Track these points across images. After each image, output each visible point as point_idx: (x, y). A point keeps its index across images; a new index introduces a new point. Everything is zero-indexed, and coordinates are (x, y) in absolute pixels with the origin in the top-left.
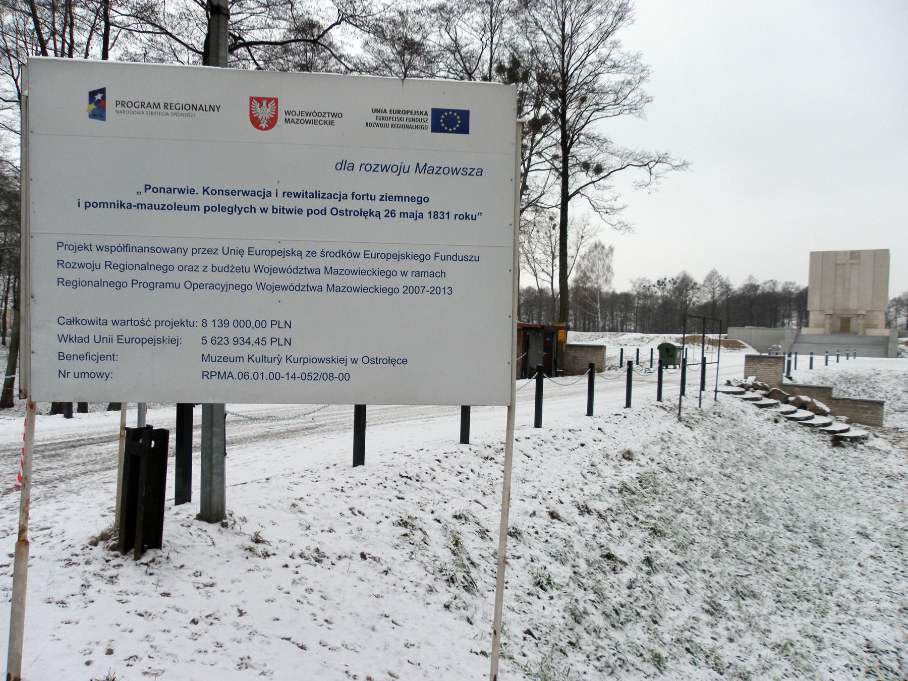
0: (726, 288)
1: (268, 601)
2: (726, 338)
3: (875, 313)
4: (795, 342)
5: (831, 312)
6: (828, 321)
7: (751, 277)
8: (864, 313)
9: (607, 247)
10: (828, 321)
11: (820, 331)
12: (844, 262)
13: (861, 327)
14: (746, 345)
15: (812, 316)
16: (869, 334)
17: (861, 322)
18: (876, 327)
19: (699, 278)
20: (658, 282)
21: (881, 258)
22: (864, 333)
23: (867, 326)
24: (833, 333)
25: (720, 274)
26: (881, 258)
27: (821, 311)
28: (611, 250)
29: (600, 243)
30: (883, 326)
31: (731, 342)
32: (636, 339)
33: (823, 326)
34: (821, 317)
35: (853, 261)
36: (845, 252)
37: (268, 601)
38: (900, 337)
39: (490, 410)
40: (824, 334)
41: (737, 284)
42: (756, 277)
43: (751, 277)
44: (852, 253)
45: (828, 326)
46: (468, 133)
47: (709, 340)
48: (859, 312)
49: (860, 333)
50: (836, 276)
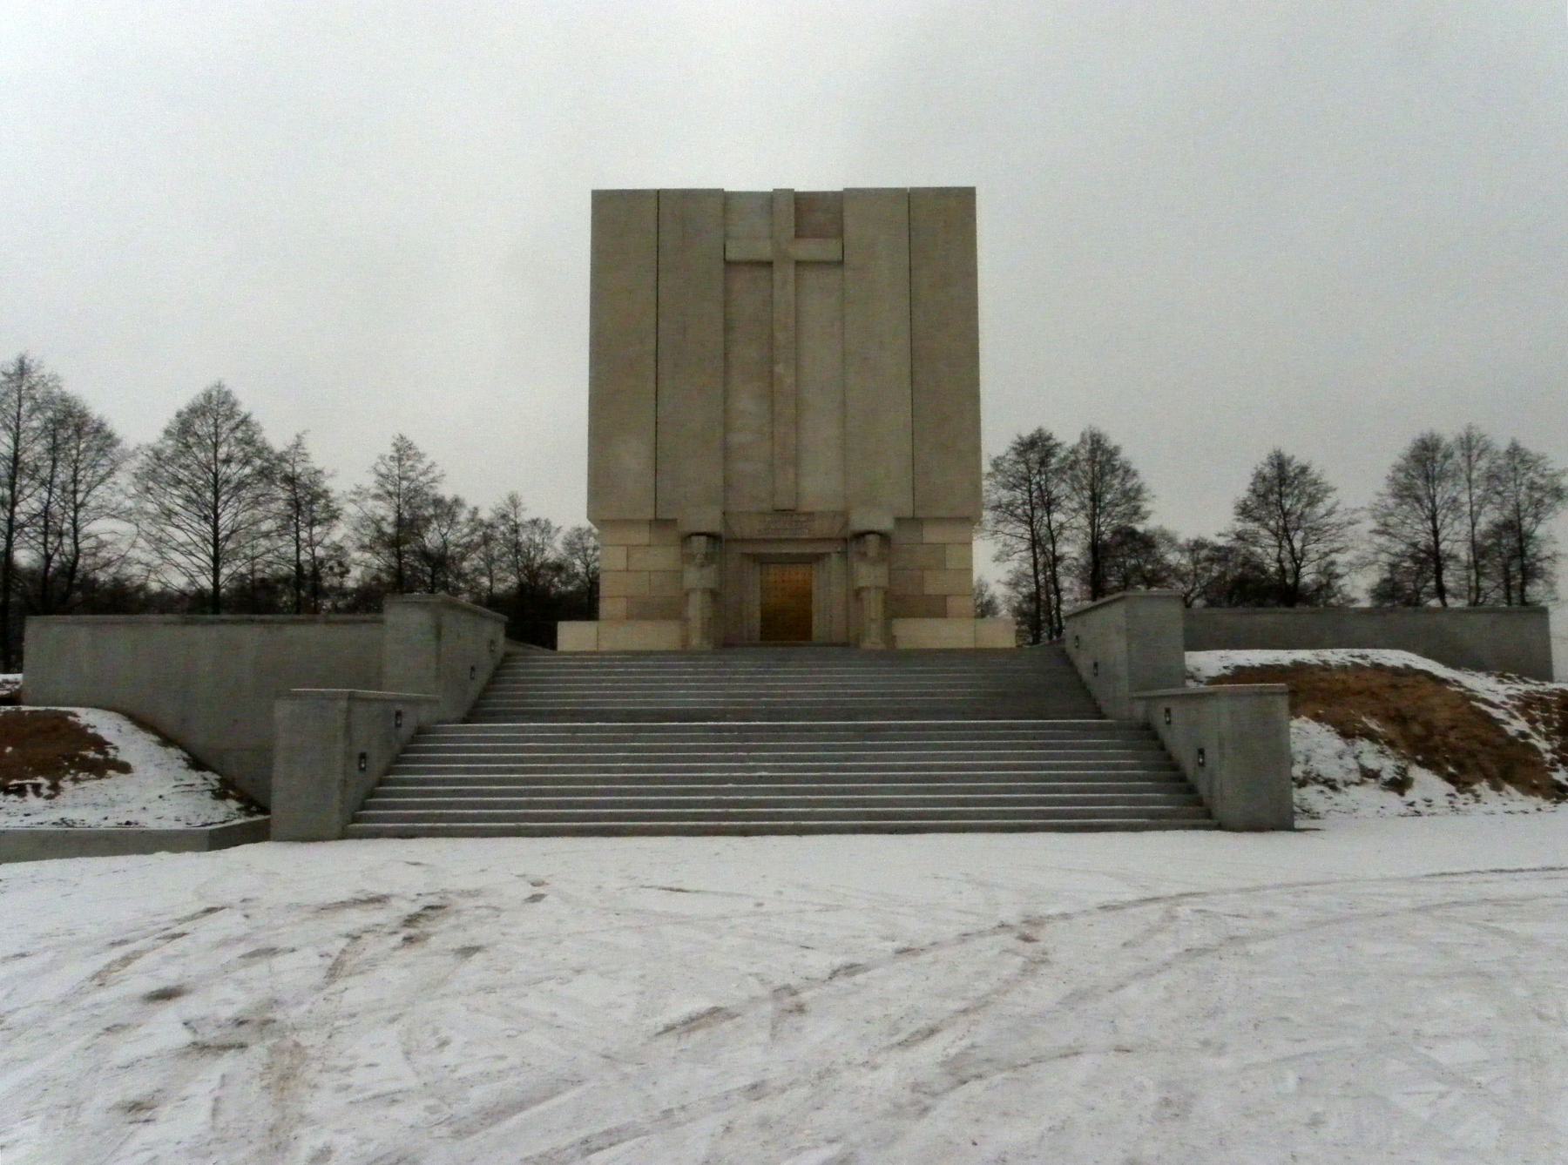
3: (932, 535)
4: (474, 714)
5: (710, 520)
6: (695, 578)
7: (404, 451)
8: (886, 524)
11: (657, 636)
12: (764, 251)
13: (874, 606)
16: (903, 645)
17: (869, 575)
21: (935, 227)
22: (891, 639)
23: (900, 604)
24: (726, 642)
26: (935, 227)
33: (671, 610)
34: (662, 557)
35: (810, 249)
36: (771, 200)
40: (684, 652)
45: (696, 609)
46: (966, 197)
50: (728, 329)
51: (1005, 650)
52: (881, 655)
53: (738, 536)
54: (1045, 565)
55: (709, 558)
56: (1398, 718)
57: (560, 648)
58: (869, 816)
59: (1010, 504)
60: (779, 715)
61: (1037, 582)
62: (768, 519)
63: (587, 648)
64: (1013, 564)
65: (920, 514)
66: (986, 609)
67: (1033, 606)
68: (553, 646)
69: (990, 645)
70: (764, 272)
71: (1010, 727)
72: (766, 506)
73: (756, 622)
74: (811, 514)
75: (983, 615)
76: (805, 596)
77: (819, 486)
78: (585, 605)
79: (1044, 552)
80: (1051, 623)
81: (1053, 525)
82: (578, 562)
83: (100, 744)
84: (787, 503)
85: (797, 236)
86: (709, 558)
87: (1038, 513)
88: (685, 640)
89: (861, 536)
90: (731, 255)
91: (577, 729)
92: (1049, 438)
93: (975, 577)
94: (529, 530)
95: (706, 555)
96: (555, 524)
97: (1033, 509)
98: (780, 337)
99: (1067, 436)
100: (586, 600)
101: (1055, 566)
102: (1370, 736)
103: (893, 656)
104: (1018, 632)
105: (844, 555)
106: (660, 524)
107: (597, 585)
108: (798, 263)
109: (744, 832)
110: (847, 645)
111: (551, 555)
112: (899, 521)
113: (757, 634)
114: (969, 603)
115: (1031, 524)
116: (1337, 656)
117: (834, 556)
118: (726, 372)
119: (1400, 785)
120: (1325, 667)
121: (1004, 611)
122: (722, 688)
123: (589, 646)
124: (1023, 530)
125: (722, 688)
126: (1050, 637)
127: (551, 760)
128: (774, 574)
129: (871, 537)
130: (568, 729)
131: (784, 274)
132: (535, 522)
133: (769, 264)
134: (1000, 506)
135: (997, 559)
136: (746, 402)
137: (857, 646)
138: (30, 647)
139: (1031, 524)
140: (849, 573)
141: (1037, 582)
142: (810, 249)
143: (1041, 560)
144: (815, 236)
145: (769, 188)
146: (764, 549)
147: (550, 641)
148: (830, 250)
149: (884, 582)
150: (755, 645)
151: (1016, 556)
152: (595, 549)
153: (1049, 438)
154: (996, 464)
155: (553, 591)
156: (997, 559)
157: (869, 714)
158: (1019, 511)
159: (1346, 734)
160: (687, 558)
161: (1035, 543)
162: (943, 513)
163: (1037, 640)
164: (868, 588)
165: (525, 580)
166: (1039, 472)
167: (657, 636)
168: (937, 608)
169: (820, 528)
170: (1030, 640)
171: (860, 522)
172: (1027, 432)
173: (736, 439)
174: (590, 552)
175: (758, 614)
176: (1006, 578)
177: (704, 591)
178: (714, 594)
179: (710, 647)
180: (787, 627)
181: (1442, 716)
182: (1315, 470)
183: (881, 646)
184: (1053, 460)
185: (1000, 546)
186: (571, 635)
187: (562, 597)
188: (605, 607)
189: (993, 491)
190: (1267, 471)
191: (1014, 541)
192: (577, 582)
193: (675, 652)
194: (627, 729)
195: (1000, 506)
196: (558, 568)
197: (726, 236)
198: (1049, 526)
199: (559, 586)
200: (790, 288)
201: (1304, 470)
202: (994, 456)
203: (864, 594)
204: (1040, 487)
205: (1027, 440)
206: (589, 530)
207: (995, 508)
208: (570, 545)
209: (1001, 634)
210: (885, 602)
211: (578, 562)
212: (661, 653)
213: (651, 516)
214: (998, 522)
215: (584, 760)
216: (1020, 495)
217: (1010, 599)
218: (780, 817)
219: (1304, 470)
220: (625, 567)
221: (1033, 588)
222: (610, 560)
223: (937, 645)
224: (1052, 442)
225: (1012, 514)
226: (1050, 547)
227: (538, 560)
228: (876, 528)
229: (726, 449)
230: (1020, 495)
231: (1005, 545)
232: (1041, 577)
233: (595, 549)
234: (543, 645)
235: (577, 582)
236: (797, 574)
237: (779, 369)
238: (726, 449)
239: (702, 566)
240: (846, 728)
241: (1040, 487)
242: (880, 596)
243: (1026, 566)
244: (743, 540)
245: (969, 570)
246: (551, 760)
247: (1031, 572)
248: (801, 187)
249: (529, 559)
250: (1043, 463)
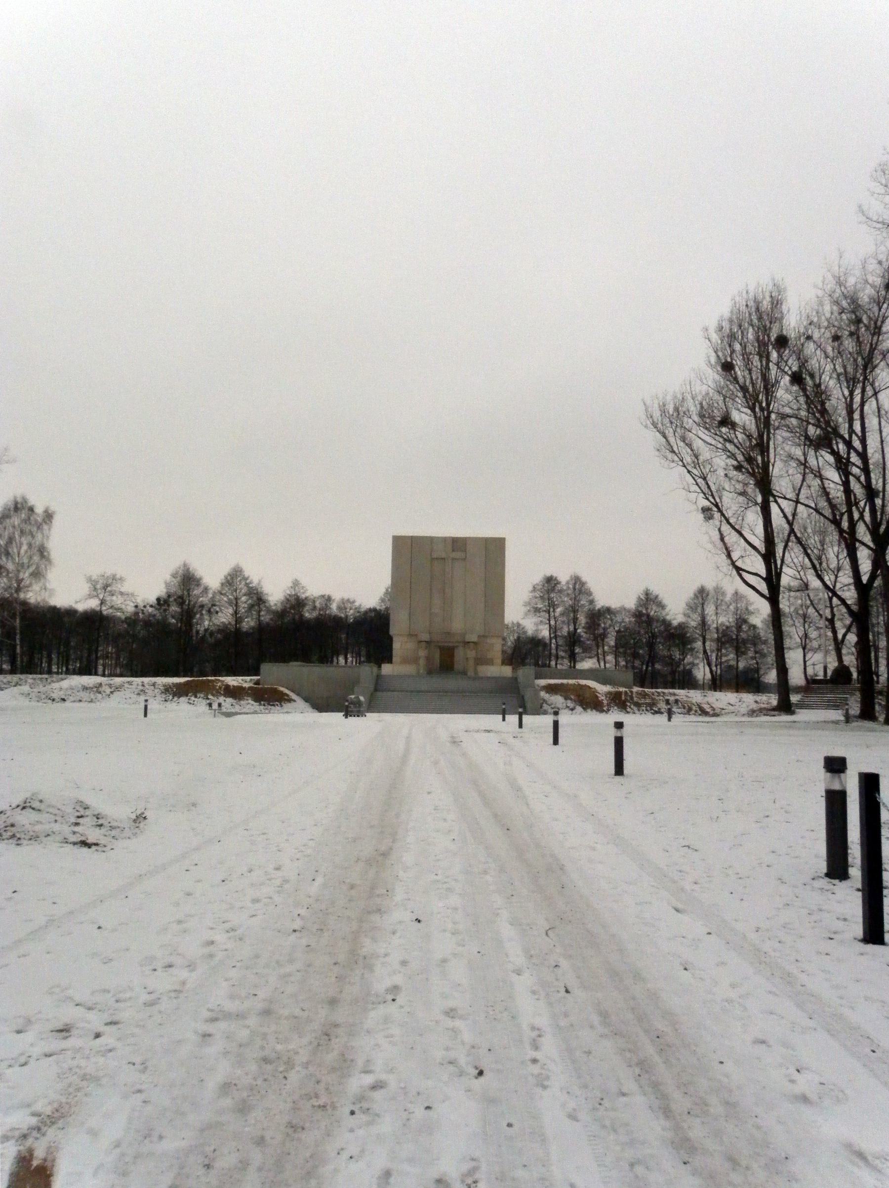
0: (258, 599)
2: (257, 683)
5: (425, 637)
7: (296, 583)
9: (39, 510)
10: (422, 653)
11: (409, 669)
12: (443, 555)
13: (471, 663)
14: (293, 696)
15: (397, 645)
16: (481, 675)
17: (471, 654)
18: (490, 662)
19: (212, 578)
20: (158, 600)
22: (476, 672)
24: (430, 672)
25: (246, 574)
27: (411, 635)
28: (49, 516)
29: (25, 501)
30: (499, 661)
31: (266, 691)
32: (85, 688)
33: (415, 660)
36: (445, 540)
38: (536, 678)
39: (300, 666)
41: (276, 593)
42: (304, 581)
43: (296, 583)
45: (422, 662)
47: (227, 687)
48: (468, 639)
49: (471, 673)
56: (579, 696)
77: (457, 625)
83: (288, 695)
99: (564, 578)
102: (571, 699)
103: (476, 678)
110: (464, 673)
116: (571, 682)
118: (431, 589)
119: (572, 710)
120: (568, 684)
133: (444, 559)
138: (262, 671)
159: (566, 699)
181: (587, 695)
182: (661, 597)
190: (642, 597)
201: (657, 597)
208: (339, 608)
219: (657, 597)
237: (447, 590)
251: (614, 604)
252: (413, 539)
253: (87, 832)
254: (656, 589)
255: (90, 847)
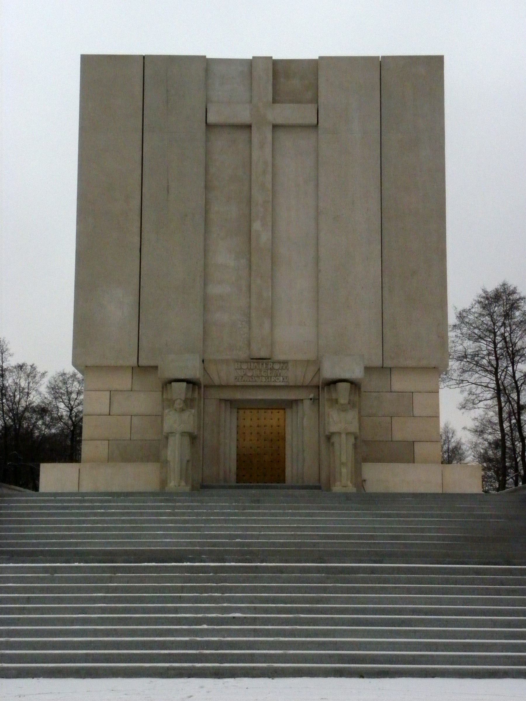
1: (191, 696)
3: (400, 383)
5: (191, 368)
8: (355, 372)
11: (138, 477)
12: (243, 115)
13: (344, 451)
16: (372, 487)
17: (341, 421)
23: (371, 449)
24: (203, 486)
33: (151, 452)
34: (143, 401)
35: (286, 113)
36: (250, 66)
37: (191, 696)
40: (162, 494)
43: (64, 370)
44: (280, 71)
45: (175, 451)
46: (440, 59)
49: (344, 484)
51: (472, 495)
52: (347, 497)
53: (217, 381)
54: (510, 414)
55: (189, 403)
57: (43, 488)
58: (342, 659)
59: (476, 354)
60: (252, 556)
61: (502, 430)
62: (244, 366)
63: (75, 491)
64: (479, 412)
65: (388, 363)
66: (453, 455)
67: (499, 454)
68: (36, 488)
69: (458, 491)
70: (241, 136)
71: (477, 572)
72: (243, 355)
73: (233, 466)
74: (285, 362)
75: (449, 461)
76: (278, 440)
77: (292, 336)
78: (67, 447)
79: (509, 401)
80: (516, 470)
81: (518, 375)
82: (62, 406)
84: (263, 354)
85: (274, 101)
86: (189, 403)
87: (503, 363)
88: (164, 482)
89: (333, 383)
90: (212, 119)
91: (55, 570)
92: (514, 292)
93: (442, 425)
94: (15, 375)
95: (185, 401)
96: (40, 369)
97: (497, 359)
98: (258, 196)
100: (69, 442)
101: (519, 414)
103: (367, 499)
104: (484, 477)
105: (316, 401)
106: (141, 370)
107: (81, 428)
108: (275, 127)
109: (218, 674)
110: (318, 487)
111: (35, 399)
112: (368, 369)
113: (233, 477)
114: (436, 451)
115: (496, 374)
117: (307, 403)
121: (470, 458)
122: (198, 529)
123: (71, 487)
124: (488, 379)
125: (198, 529)
126: (516, 484)
127: (29, 600)
128: (250, 419)
129: (342, 386)
130: (46, 570)
131: (262, 136)
132: (21, 367)
134: (465, 356)
135: (463, 407)
136: (225, 256)
137: (329, 489)
139: (496, 374)
140: (320, 416)
141: (502, 430)
142: (286, 113)
143: (506, 409)
144: (292, 102)
145: (249, 56)
146: (238, 395)
147: (32, 482)
148: (302, 114)
149: (354, 428)
150: (230, 487)
151: (481, 404)
152: (79, 393)
153: (514, 292)
154: (461, 317)
155: (37, 433)
156: (463, 407)
157: (341, 556)
158: (485, 362)
160: (169, 403)
161: (500, 391)
162: (410, 363)
163: (502, 486)
164: (340, 433)
165: (10, 422)
166: (504, 324)
167: (138, 477)
168: (404, 453)
169: (295, 375)
170: (497, 485)
171: (330, 371)
172: (491, 287)
173: (214, 290)
174: (74, 396)
175: (234, 456)
176: (471, 424)
177: (183, 434)
178: (193, 438)
179: (188, 489)
180: (261, 469)
183: (351, 489)
184: (517, 313)
185: (466, 394)
186: (53, 476)
187: (45, 438)
188: (87, 449)
189: (458, 342)
191: (479, 390)
192: (60, 425)
193: (153, 494)
194: (104, 570)
195: (465, 356)
196: (42, 411)
197: (208, 101)
198: (514, 377)
199: (42, 428)
200: (268, 149)
202: (460, 309)
203: (335, 439)
204: (504, 338)
205: (492, 295)
206: (74, 376)
207: (460, 359)
208: (54, 389)
209: (467, 479)
210: (355, 446)
211: (62, 406)
212: (140, 494)
213: (133, 362)
214: (464, 371)
215: (60, 600)
216: (484, 346)
217: (476, 445)
218: (252, 658)
220: (109, 412)
221: (499, 436)
222: (93, 405)
223: (405, 489)
224: (516, 296)
225: (477, 364)
226: (514, 396)
227: (23, 404)
228: (347, 375)
229: (206, 300)
230: (484, 346)
231: (471, 393)
232: (506, 425)
233: (79, 393)
234: (25, 486)
235: (60, 425)
236: (272, 419)
237: (257, 226)
238: (206, 300)
239: (182, 410)
240: (318, 570)
241: (504, 338)
242: (352, 440)
243: (491, 413)
244: (221, 387)
245: (436, 417)
246: (29, 600)
247: (496, 420)
248: (276, 56)
249: (14, 403)
250: (507, 315)
251: (467, 306)
252: (146, 66)
253: (21, 491)
254: (512, 283)
255: (320, 271)
